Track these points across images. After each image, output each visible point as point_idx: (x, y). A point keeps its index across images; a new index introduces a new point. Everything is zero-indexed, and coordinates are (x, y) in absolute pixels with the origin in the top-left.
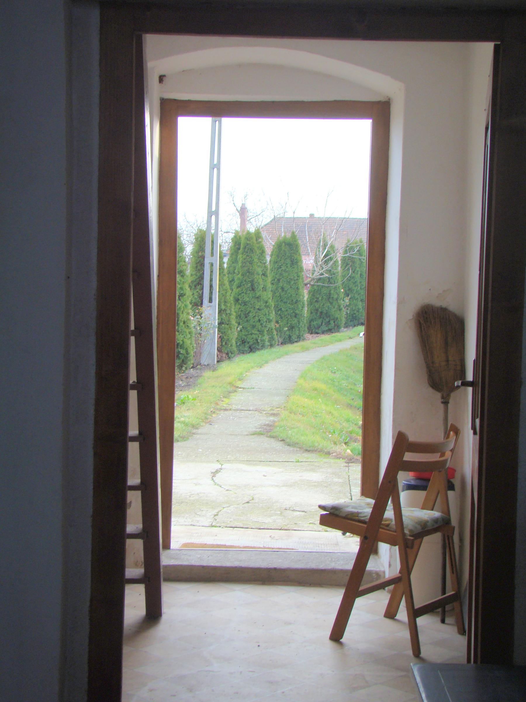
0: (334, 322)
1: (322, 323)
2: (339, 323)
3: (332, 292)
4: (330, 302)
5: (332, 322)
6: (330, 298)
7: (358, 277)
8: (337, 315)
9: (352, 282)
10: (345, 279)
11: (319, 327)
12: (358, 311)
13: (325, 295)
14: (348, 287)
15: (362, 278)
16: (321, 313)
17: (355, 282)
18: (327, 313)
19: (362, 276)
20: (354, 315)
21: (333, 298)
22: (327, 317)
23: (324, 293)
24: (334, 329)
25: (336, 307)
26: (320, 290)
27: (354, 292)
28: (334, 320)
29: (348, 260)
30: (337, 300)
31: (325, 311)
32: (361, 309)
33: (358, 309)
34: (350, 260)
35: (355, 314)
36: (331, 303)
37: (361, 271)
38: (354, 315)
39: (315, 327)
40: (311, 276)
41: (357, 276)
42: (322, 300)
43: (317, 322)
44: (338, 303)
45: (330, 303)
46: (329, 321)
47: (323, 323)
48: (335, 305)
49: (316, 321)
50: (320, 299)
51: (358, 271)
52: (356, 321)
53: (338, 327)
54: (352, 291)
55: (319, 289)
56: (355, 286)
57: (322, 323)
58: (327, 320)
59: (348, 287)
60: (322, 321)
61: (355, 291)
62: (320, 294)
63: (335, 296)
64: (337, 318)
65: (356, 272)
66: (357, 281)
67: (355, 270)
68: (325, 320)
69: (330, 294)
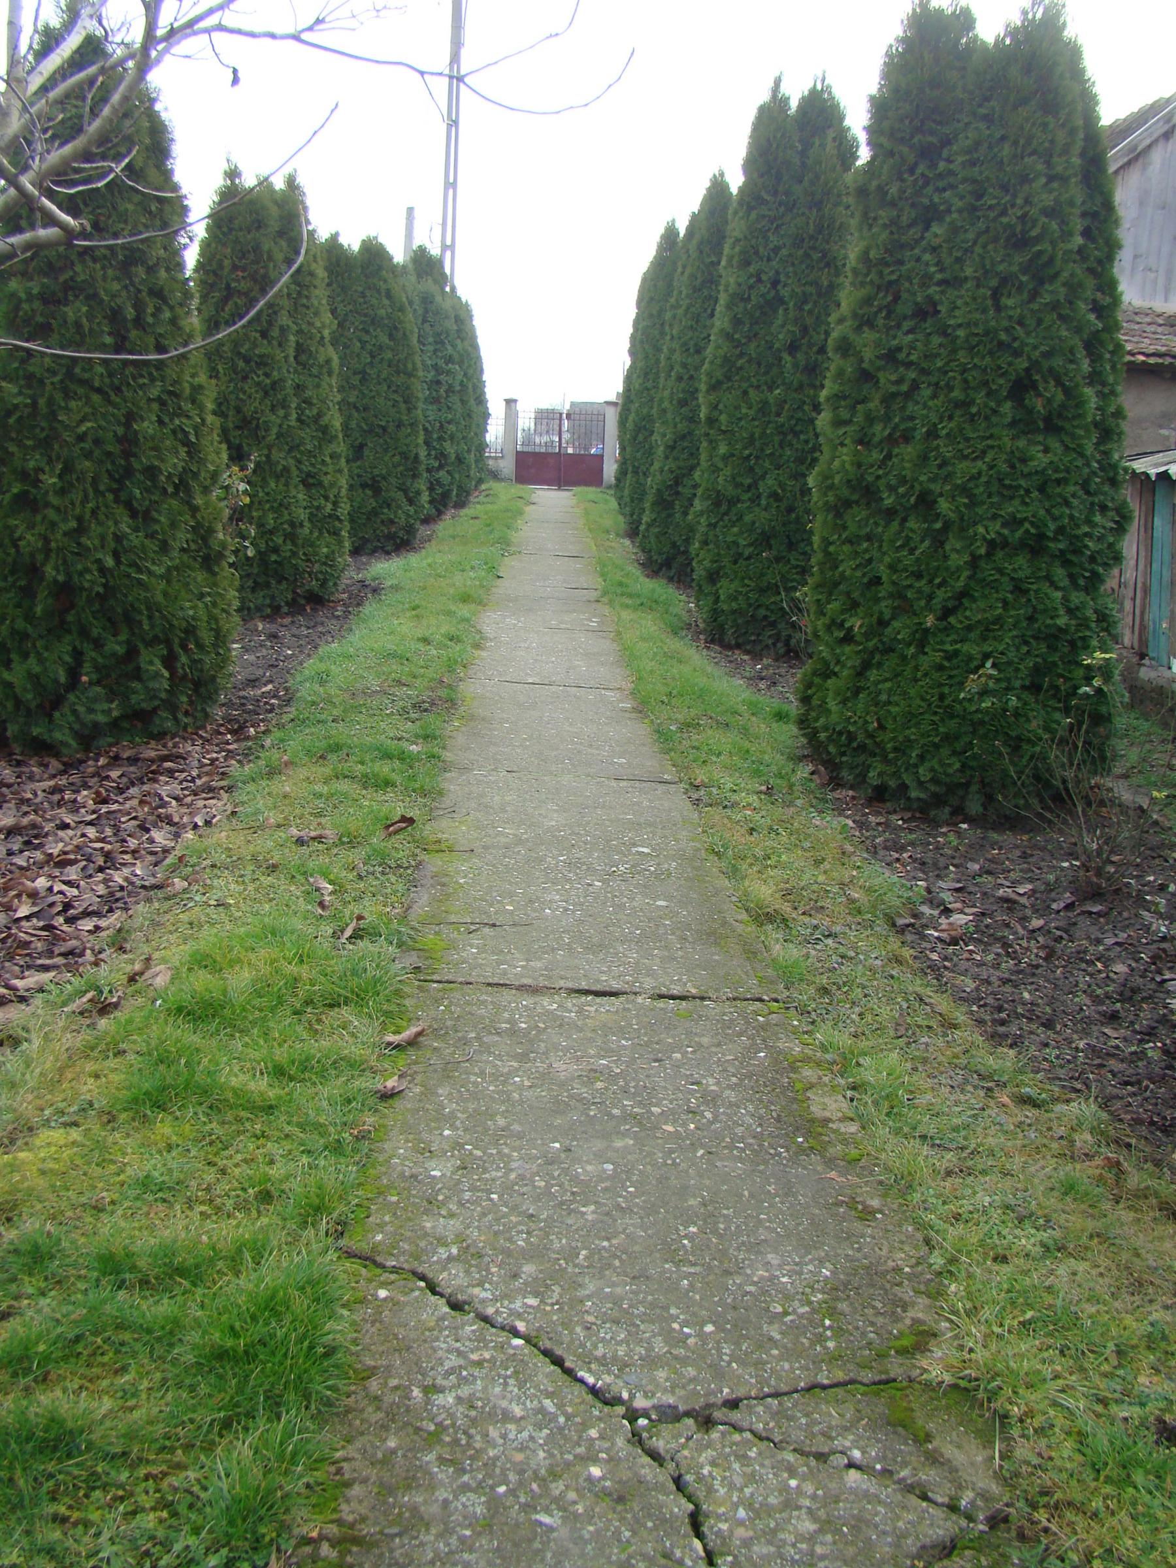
0: (169, 661)
1: (74, 674)
2: (208, 660)
3: (147, 426)
4: (128, 505)
5: (152, 662)
6: (129, 472)
7: (286, 358)
8: (189, 609)
9: (258, 384)
10: (285, 278)
11: (52, 703)
12: (291, 537)
13: (88, 455)
14: (238, 411)
15: (304, 366)
16: (65, 592)
17: (274, 383)
18: (110, 591)
19: (303, 358)
20: (274, 557)
21: (152, 472)
22: (113, 626)
23: (81, 438)
24: (173, 708)
25: (182, 537)
26: (53, 415)
27: (272, 437)
28: (168, 643)
29: (235, 268)
30: (182, 485)
31: (92, 581)
32: (306, 524)
33: (292, 524)
34: (244, 270)
35: (276, 550)
36: (142, 516)
37: (300, 332)
38: (274, 557)
39: (18, 703)
40: (813, 952)
41: (279, 355)
42: (62, 492)
43: (32, 661)
44: (194, 510)
45: (134, 514)
46: (132, 653)
47: (87, 667)
48: (173, 525)
49: (25, 656)
50: (51, 480)
51: (284, 330)
52: (284, 585)
53: (197, 685)
54: (262, 433)
55: (42, 402)
56: (273, 408)
57: (74, 674)
58: (115, 646)
59: (238, 411)
60: (78, 654)
61: (275, 430)
62: (45, 444)
63: (173, 462)
64: (190, 631)
65: (275, 333)
66: (282, 380)
67: (270, 323)
68: (98, 644)
69: (129, 443)
